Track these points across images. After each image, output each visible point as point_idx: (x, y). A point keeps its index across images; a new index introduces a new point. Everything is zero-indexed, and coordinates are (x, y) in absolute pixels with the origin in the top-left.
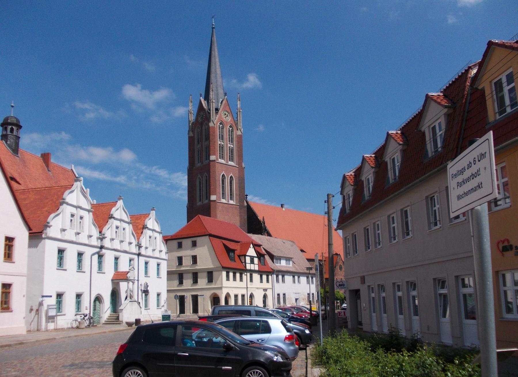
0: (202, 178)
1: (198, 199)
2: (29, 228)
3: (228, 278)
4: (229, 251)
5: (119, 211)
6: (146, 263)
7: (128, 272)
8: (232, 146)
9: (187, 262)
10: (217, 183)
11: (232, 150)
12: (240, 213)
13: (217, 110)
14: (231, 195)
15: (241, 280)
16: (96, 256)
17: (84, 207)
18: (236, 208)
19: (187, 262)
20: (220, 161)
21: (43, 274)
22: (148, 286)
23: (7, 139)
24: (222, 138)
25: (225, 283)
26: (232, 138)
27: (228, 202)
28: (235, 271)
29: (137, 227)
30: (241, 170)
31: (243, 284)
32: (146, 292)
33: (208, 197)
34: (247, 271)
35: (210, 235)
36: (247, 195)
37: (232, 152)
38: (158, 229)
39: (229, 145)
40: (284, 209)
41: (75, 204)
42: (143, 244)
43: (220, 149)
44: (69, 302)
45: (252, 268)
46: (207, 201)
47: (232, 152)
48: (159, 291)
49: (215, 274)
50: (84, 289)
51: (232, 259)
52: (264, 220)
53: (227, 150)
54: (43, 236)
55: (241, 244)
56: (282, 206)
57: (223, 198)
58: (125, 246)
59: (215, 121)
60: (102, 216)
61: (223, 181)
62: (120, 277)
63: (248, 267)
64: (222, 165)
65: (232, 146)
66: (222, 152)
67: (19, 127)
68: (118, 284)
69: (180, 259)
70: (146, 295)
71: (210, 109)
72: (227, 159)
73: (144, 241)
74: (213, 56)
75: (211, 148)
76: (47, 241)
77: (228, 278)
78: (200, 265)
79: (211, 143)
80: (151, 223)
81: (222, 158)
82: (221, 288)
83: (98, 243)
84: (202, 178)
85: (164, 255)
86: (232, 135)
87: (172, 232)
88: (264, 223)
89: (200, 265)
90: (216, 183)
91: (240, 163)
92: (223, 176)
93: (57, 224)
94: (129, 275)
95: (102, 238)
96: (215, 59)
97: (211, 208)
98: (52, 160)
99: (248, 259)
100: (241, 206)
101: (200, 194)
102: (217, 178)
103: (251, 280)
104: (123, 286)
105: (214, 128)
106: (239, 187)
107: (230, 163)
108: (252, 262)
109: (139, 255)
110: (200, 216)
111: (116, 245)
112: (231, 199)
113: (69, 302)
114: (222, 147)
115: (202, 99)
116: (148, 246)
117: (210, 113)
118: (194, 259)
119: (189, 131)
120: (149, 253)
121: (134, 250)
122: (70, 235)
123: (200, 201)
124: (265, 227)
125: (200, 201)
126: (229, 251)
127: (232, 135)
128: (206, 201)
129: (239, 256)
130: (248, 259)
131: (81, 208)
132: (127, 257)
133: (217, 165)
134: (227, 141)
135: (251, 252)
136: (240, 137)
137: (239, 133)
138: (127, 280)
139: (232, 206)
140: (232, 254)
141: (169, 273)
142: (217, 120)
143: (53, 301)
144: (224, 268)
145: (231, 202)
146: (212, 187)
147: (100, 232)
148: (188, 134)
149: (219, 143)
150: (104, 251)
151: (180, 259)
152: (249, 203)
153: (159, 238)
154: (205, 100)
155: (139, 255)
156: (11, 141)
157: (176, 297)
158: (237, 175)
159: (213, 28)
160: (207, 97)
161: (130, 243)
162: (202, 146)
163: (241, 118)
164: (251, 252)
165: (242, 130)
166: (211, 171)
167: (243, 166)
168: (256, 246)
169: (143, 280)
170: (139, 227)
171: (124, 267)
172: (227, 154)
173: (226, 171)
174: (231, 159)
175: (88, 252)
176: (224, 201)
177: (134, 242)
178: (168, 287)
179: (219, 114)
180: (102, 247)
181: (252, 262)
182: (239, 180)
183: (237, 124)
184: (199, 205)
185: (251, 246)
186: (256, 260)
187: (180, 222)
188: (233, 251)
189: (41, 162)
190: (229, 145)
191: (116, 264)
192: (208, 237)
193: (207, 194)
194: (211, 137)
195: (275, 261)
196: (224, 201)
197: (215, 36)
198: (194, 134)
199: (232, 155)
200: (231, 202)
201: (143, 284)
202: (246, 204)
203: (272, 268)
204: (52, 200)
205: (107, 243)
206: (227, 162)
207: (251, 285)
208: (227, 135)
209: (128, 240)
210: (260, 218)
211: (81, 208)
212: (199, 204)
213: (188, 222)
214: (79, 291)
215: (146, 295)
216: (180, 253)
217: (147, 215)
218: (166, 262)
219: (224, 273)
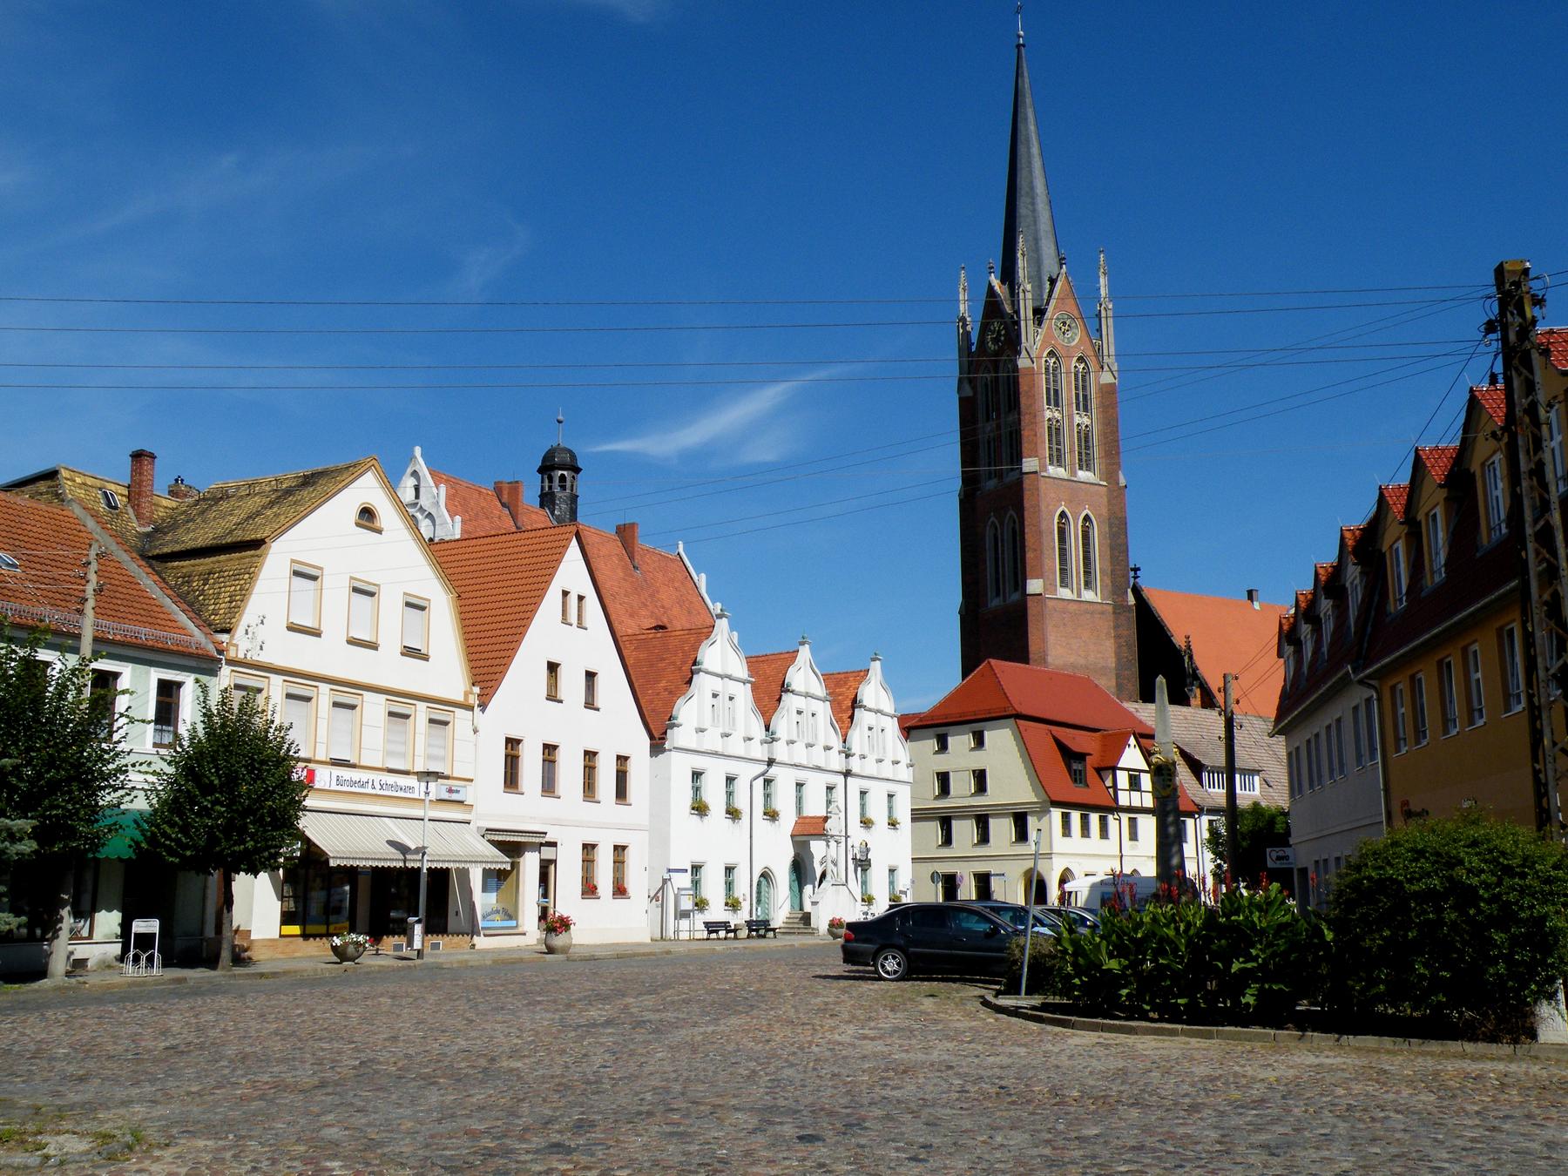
0: (1002, 524)
1: (990, 592)
2: (652, 737)
3: (1067, 830)
4: (1071, 757)
5: (803, 676)
6: (863, 793)
7: (826, 819)
8: (1086, 421)
9: (962, 786)
10: (1045, 540)
11: (1085, 437)
12: (1116, 627)
13: (1039, 313)
14: (1087, 573)
15: (1104, 833)
16: (761, 780)
17: (735, 675)
18: (1102, 613)
19: (962, 786)
20: (1053, 471)
21: (669, 824)
22: (868, 850)
23: (554, 504)
24: (1055, 399)
25: (1059, 843)
26: (1085, 397)
27: (1079, 595)
28: (1086, 808)
29: (839, 704)
30: (1117, 494)
31: (1111, 845)
32: (863, 864)
33: (1020, 582)
34: (1116, 809)
35: (1019, 716)
36: (1136, 570)
37: (1087, 441)
38: (888, 707)
39: (1077, 419)
40: (1257, 605)
41: (719, 671)
42: (855, 749)
43: (1050, 435)
44: (1332, 864)
45: (1136, 803)
46: (1015, 597)
47: (1087, 441)
48: (893, 863)
49: (1032, 822)
50: (740, 858)
51: (1078, 777)
52: (1189, 647)
53: (1071, 436)
54: (667, 746)
55: (1104, 737)
56: (1250, 595)
57: (1064, 584)
58: (818, 757)
59: (1035, 343)
60: (769, 690)
61: (1062, 532)
62: (809, 831)
63: (1124, 799)
64: (1061, 484)
65: (1086, 421)
66: (1058, 443)
67: (577, 470)
68: (806, 845)
69: (944, 778)
70: (864, 870)
71: (1017, 312)
72: (1072, 464)
73: (857, 737)
74: (1021, 137)
75: (1025, 433)
76: (674, 754)
77: (1067, 830)
78: (997, 794)
79: (1025, 420)
80: (873, 693)
81: (1058, 459)
82: (1049, 856)
83: (761, 752)
84: (1002, 524)
85: (905, 773)
86: (1084, 387)
87: (924, 703)
88: (1191, 658)
89: (997, 794)
90: (1041, 543)
91: (1110, 475)
92: (1063, 515)
93: (690, 712)
94: (827, 826)
95: (771, 737)
96: (1029, 148)
97: (1030, 618)
98: (642, 542)
99: (1123, 779)
100: (1119, 608)
101: (997, 572)
102: (1044, 526)
103: (1134, 836)
104: (817, 848)
105: (1031, 371)
106: (1112, 548)
107: (1083, 475)
108: (1135, 784)
109: (847, 774)
110: (993, 661)
111: (800, 754)
112: (1088, 585)
113: (1332, 864)
114: (1055, 431)
115: (996, 283)
116: (866, 752)
117: (1018, 323)
118: (980, 777)
119: (960, 381)
120: (870, 768)
121: (837, 762)
122: (712, 741)
123: (998, 594)
124: (1195, 670)
125: (998, 594)
126: (1071, 757)
127: (1084, 387)
128: (1015, 597)
129: (1099, 770)
130: (1123, 779)
131: (729, 677)
132: (821, 780)
133: (1043, 485)
134: (1070, 405)
135: (1132, 757)
136: (1108, 391)
137: (1106, 378)
138: (822, 835)
139: (1091, 608)
140: (1075, 766)
141: (918, 816)
142: (1039, 344)
143: (684, 880)
144: (1056, 804)
145: (1088, 595)
146: (1029, 555)
147: (767, 728)
148: (959, 389)
149: (1048, 414)
150: (773, 771)
151: (944, 778)
152: (1145, 594)
153: (892, 727)
154: (1003, 282)
155: (847, 774)
156: (561, 508)
157: (934, 877)
158: (1104, 511)
159: (1019, 46)
160: (1009, 275)
161: (828, 748)
162: (999, 427)
163: (1112, 340)
164: (1132, 757)
165: (1115, 368)
166: (1027, 504)
167: (1122, 482)
168: (1145, 738)
169: (858, 835)
170: (846, 708)
171: (815, 808)
172: (1072, 451)
173: (1069, 502)
174: (1085, 463)
175: (746, 772)
176: (1065, 593)
177: (836, 742)
178: (913, 851)
179: (1046, 324)
180: (771, 762)
181: (1135, 784)
182: (1110, 526)
183: (1098, 352)
184: (995, 624)
185: (1132, 741)
186: (1146, 781)
187: (941, 676)
188: (1081, 757)
189: (616, 547)
190: (1077, 419)
191: (799, 800)
192: (1012, 721)
193: (1016, 574)
194: (1023, 400)
195: (1205, 775)
196: (1065, 593)
197: (1028, 100)
198: (974, 388)
199: (1087, 448)
200: (1088, 595)
201: (857, 845)
202: (1131, 600)
203: (1197, 800)
204: (674, 663)
205: (780, 751)
206: (1074, 473)
207: (1133, 848)
208: (1069, 390)
209: (821, 743)
210: (1179, 641)
211: (729, 677)
212: (995, 603)
213: (965, 675)
214: (731, 861)
215: (864, 870)
216: (943, 763)
217: (863, 675)
218: (908, 788)
219: (1056, 814)
